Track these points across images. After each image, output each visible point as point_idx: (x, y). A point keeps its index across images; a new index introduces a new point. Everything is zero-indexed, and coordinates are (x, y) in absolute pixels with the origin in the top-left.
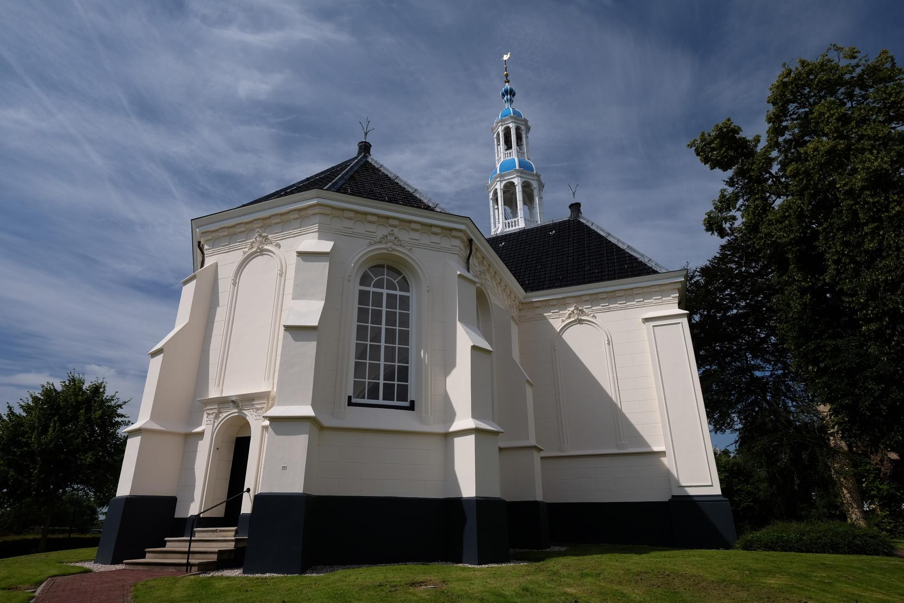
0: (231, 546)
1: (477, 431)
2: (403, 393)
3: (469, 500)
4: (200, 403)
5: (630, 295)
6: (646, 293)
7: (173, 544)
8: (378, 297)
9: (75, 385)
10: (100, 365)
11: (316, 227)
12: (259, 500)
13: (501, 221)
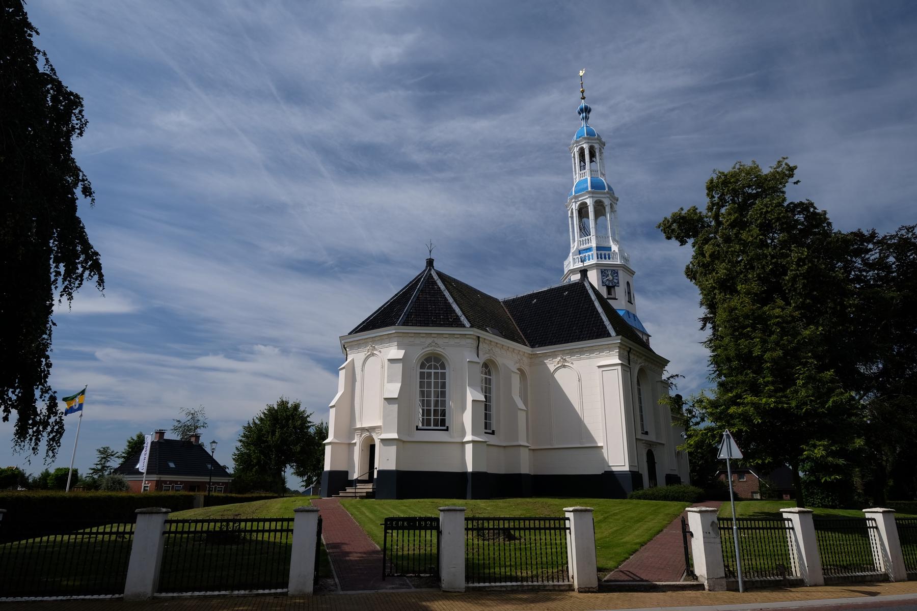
1: (473, 442)
2: (443, 422)
3: (622, 474)
4: (352, 430)
5: (591, 350)
6: (600, 349)
7: (349, 490)
8: (429, 374)
9: (283, 404)
10: (265, 345)
11: (396, 344)
12: (378, 472)
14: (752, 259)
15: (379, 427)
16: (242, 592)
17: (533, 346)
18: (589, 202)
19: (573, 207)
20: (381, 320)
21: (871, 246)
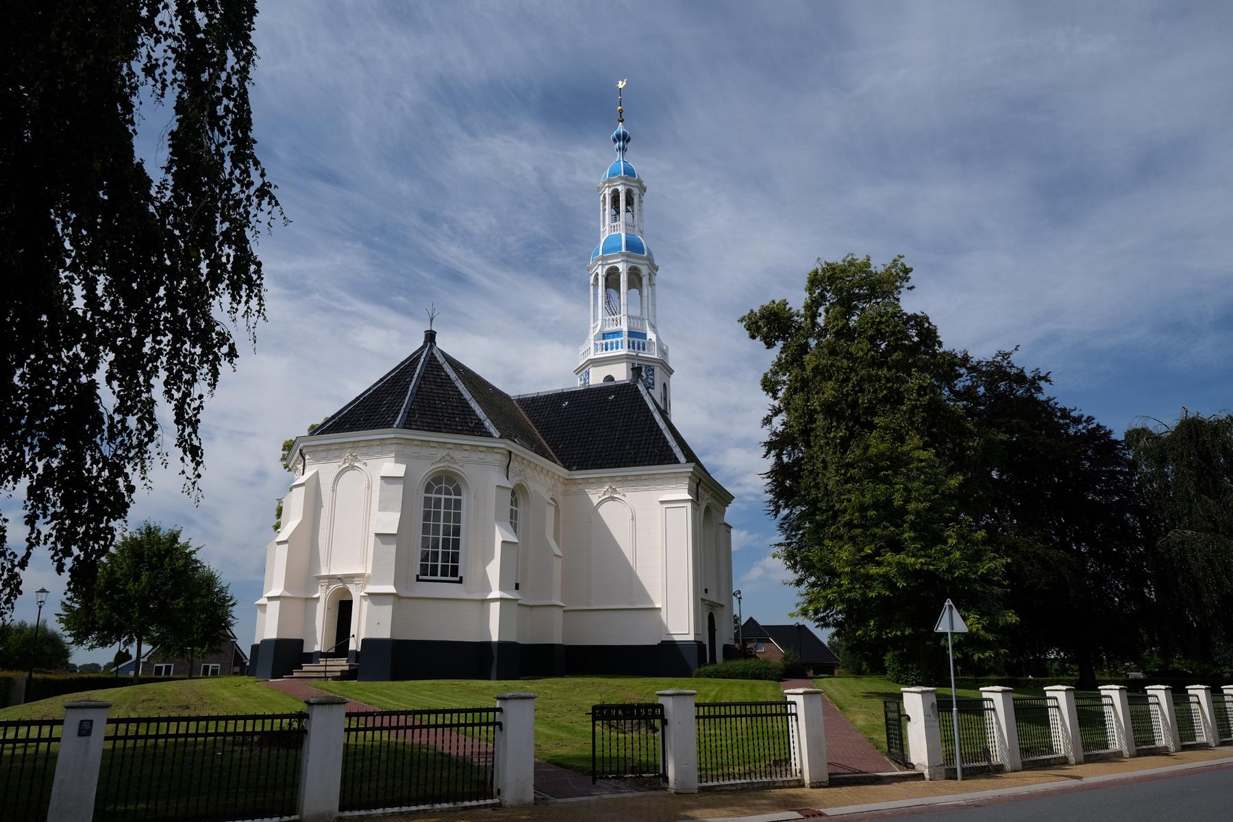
0: (347, 668)
1: (501, 599)
2: (455, 571)
3: (686, 644)
5: (652, 480)
8: (438, 501)
13: (600, 317)
14: (862, 379)
15: (361, 576)
16: (445, 805)
17: (569, 468)
18: (622, 267)
19: (599, 271)
20: (363, 416)
21: (963, 371)
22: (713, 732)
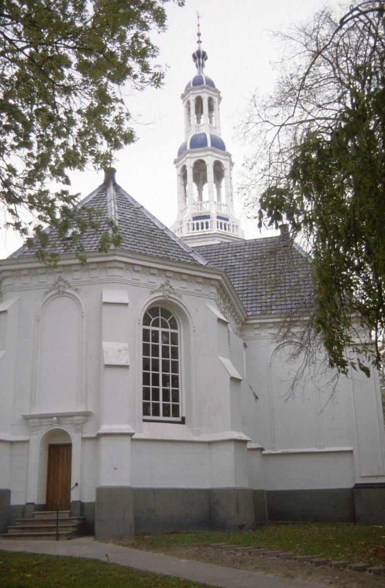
2: (176, 412)
8: (156, 333)
22: (274, 307)
